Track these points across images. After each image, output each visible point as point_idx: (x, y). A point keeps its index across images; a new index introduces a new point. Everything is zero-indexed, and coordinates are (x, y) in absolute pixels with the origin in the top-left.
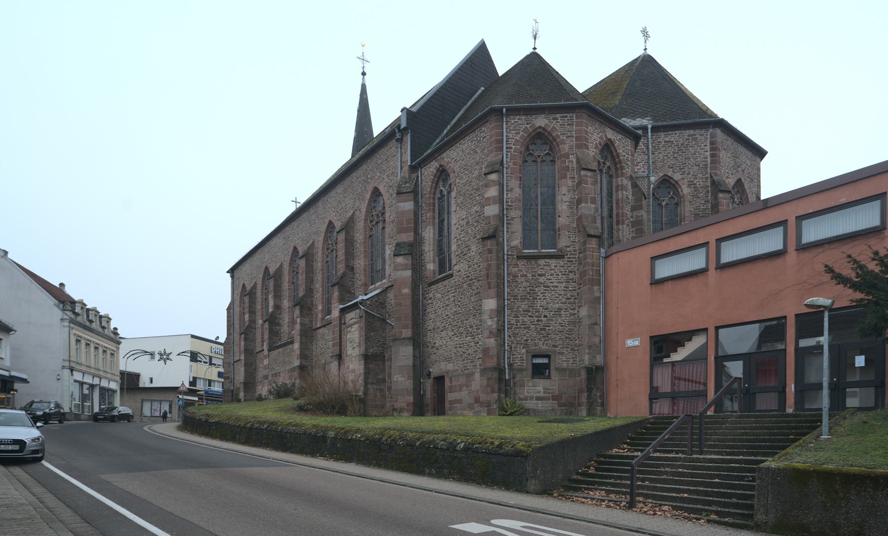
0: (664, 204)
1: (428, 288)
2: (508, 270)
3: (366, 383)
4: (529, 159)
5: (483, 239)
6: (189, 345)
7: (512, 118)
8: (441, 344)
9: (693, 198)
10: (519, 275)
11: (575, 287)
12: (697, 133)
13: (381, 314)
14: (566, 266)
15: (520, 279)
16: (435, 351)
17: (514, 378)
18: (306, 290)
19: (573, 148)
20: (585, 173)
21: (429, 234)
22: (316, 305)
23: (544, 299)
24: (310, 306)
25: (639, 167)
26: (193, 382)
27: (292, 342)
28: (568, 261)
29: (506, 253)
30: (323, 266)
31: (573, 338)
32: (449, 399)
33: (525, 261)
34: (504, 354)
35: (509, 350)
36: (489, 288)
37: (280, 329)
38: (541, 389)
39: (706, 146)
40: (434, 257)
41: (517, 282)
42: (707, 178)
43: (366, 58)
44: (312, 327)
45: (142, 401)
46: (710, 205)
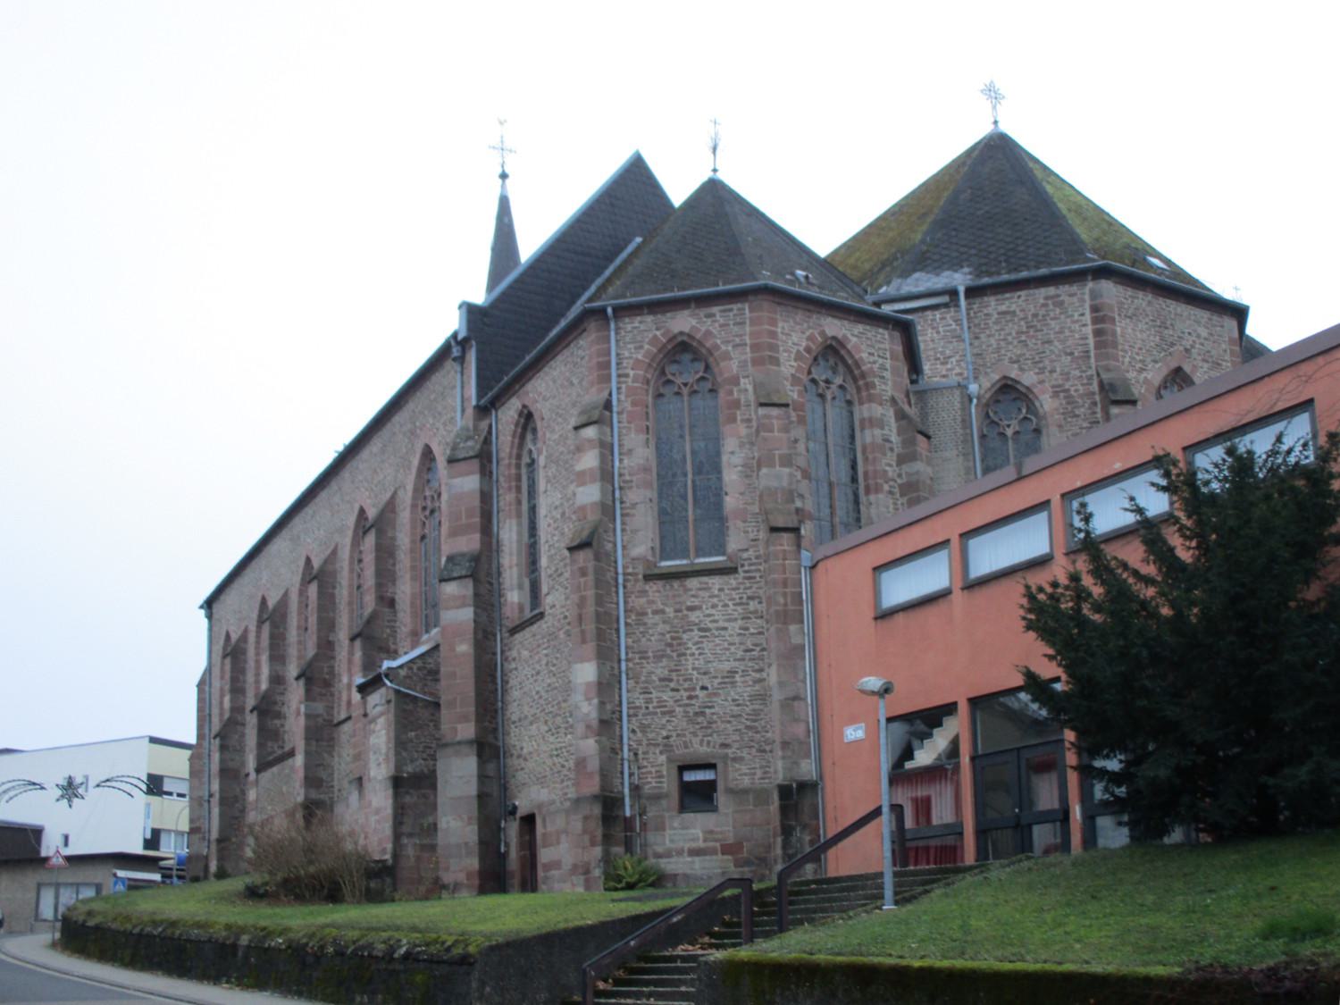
0: (1009, 432)
2: (626, 602)
3: (397, 836)
4: (667, 391)
5: (571, 549)
6: (140, 766)
8: (531, 749)
10: (649, 611)
12: (1063, 290)
15: (651, 619)
18: (319, 646)
19: (747, 366)
21: (510, 534)
23: (700, 654)
24: (327, 677)
25: (949, 366)
26: (153, 841)
28: (745, 578)
29: (620, 570)
30: (351, 595)
33: (660, 583)
34: (622, 768)
35: (632, 758)
36: (584, 641)
37: (283, 726)
39: (1083, 315)
40: (520, 577)
41: (645, 624)
42: (1090, 378)
43: (507, 145)
44: (332, 721)
45: (39, 886)
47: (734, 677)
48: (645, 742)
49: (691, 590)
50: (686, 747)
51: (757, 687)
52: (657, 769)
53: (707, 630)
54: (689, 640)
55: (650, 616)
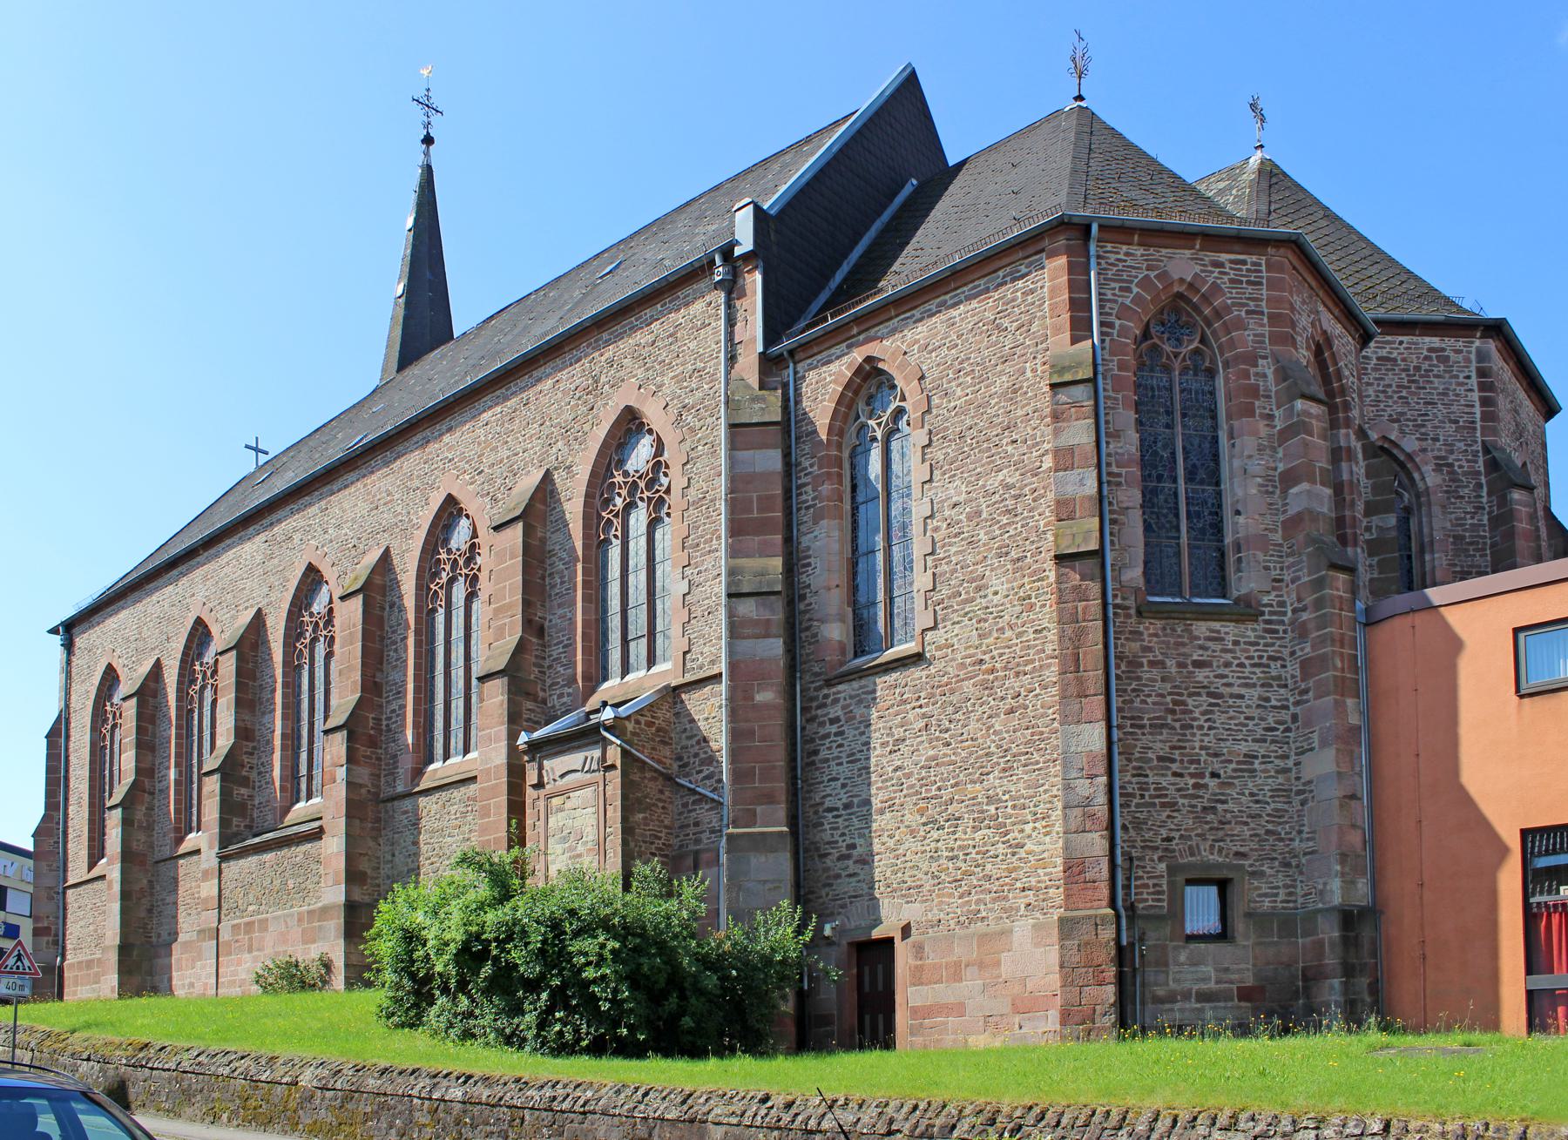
1: (825, 691)
7: (1109, 249)
9: (1448, 498)
10: (1145, 661)
11: (1287, 700)
13: (659, 762)
14: (1262, 641)
15: (1146, 673)
16: (853, 868)
17: (1142, 940)
20: (1305, 407)
22: (389, 730)
23: (1210, 728)
24: (372, 732)
27: (317, 835)
28: (1266, 631)
31: (1286, 833)
32: (915, 1002)
35: (1127, 865)
37: (251, 797)
38: (1208, 970)
39: (1468, 377)
41: (1139, 678)
42: (1475, 453)
44: (377, 794)
46: (1486, 517)
47: (1252, 763)
48: (1139, 844)
49: (1198, 638)
50: (1192, 854)
51: (1281, 779)
52: (1155, 881)
53: (1220, 696)
54: (1196, 707)
55: (1146, 668)
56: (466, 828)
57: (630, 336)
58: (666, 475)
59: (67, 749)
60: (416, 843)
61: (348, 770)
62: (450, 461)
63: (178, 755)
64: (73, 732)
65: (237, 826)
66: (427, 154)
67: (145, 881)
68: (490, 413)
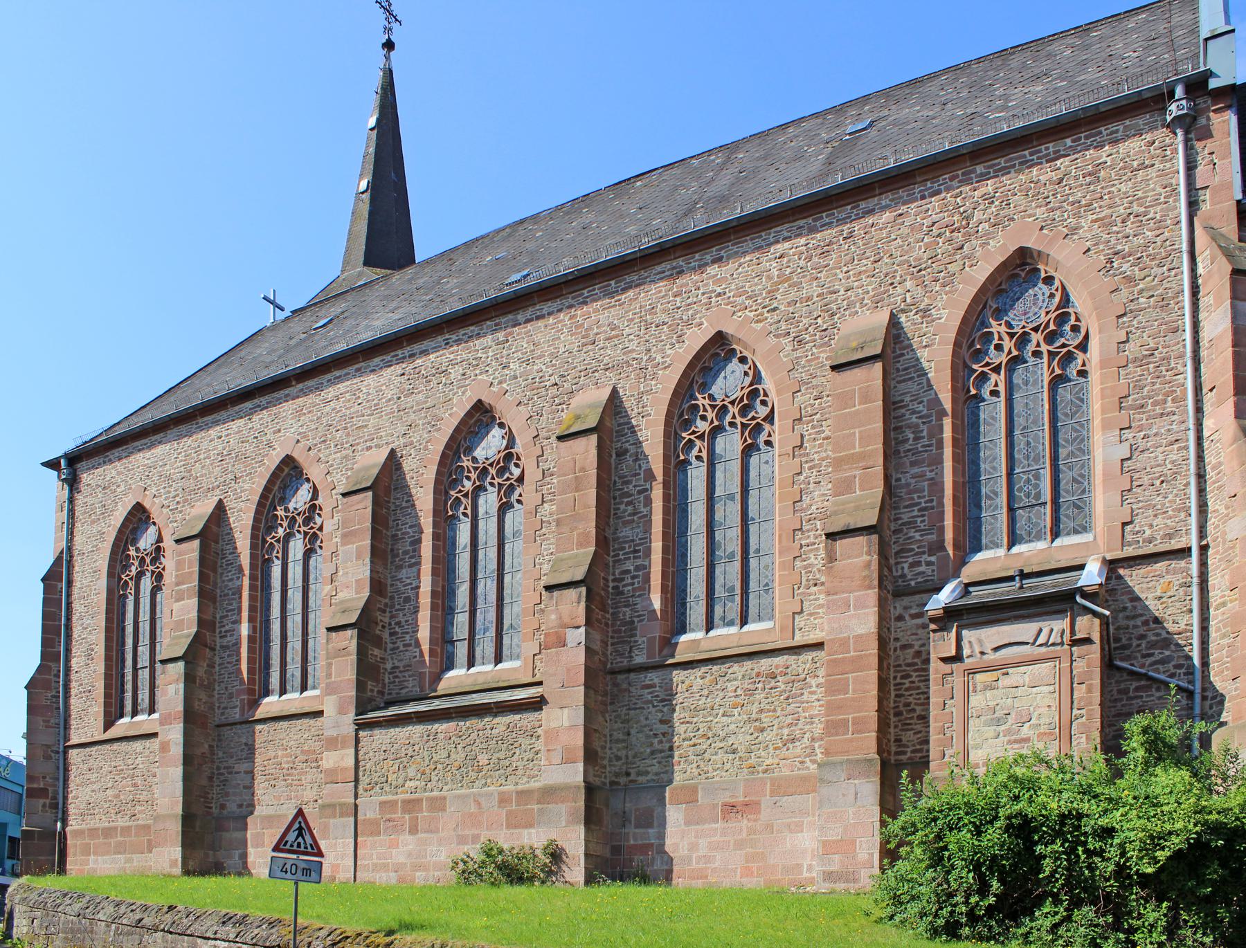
56: (755, 708)
57: (1019, 171)
58: (319, 515)
59: (69, 595)
60: (667, 722)
61: (587, 633)
62: (719, 295)
63: (252, 609)
64: (77, 577)
65: (372, 691)
66: (387, 58)
67: (207, 746)
68: (787, 245)
